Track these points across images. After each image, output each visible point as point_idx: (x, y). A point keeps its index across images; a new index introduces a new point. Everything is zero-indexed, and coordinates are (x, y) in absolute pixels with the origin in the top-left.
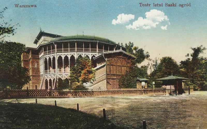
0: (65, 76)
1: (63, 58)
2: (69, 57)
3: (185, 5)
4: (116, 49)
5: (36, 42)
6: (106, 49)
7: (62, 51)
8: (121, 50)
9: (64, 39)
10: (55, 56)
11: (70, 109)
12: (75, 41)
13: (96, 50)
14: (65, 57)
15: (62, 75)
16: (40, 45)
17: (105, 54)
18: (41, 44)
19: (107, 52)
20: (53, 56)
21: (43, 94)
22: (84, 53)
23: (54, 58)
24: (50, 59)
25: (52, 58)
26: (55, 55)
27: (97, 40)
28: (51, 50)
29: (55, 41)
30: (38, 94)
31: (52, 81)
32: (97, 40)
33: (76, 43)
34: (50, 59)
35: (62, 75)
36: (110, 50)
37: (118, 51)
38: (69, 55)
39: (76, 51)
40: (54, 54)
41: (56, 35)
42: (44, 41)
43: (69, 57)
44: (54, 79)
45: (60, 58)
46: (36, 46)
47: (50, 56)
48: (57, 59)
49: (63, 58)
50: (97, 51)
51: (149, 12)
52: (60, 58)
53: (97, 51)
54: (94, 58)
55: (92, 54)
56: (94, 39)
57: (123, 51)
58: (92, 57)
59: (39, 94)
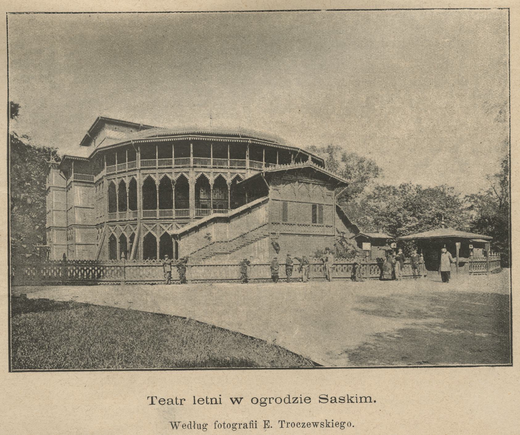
0: (163, 227)
1: (157, 183)
2: (157, 180)
3: (273, 401)
4: (297, 161)
5: (86, 142)
6: (270, 160)
7: (155, 165)
8: (309, 163)
9: (160, 136)
10: (137, 179)
11: (66, 369)
12: (190, 139)
13: (244, 163)
14: (216, 181)
15: (154, 225)
16: (96, 150)
17: (266, 173)
18: (100, 147)
19: (273, 168)
20: (131, 178)
21: (88, 271)
22: (157, 171)
23: (133, 183)
24: (122, 184)
25: (127, 181)
26: (136, 175)
27: (247, 137)
28: (127, 163)
29: (136, 140)
30: (91, 270)
31: (128, 240)
32: (247, 137)
33: (192, 146)
34: (122, 184)
35: (154, 225)
36: (280, 164)
37: (301, 165)
38: (157, 175)
39: (192, 165)
40: (133, 173)
41: (139, 125)
42: (111, 137)
43: (157, 180)
44: (133, 235)
45: (149, 182)
46: (85, 153)
47: (124, 179)
48: (142, 186)
49: (157, 183)
50: (248, 166)
51: (427, 182)
52: (149, 182)
53: (248, 166)
54: (238, 182)
55: (146, 174)
56: (238, 136)
57: (315, 166)
58: (234, 181)
59: (90, 271)
